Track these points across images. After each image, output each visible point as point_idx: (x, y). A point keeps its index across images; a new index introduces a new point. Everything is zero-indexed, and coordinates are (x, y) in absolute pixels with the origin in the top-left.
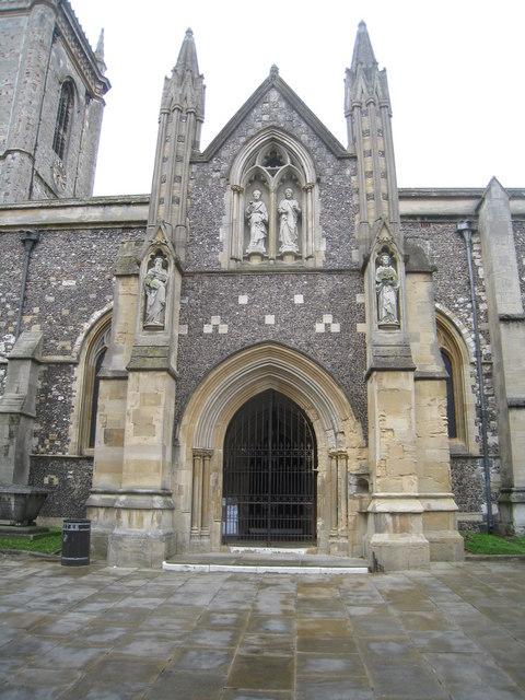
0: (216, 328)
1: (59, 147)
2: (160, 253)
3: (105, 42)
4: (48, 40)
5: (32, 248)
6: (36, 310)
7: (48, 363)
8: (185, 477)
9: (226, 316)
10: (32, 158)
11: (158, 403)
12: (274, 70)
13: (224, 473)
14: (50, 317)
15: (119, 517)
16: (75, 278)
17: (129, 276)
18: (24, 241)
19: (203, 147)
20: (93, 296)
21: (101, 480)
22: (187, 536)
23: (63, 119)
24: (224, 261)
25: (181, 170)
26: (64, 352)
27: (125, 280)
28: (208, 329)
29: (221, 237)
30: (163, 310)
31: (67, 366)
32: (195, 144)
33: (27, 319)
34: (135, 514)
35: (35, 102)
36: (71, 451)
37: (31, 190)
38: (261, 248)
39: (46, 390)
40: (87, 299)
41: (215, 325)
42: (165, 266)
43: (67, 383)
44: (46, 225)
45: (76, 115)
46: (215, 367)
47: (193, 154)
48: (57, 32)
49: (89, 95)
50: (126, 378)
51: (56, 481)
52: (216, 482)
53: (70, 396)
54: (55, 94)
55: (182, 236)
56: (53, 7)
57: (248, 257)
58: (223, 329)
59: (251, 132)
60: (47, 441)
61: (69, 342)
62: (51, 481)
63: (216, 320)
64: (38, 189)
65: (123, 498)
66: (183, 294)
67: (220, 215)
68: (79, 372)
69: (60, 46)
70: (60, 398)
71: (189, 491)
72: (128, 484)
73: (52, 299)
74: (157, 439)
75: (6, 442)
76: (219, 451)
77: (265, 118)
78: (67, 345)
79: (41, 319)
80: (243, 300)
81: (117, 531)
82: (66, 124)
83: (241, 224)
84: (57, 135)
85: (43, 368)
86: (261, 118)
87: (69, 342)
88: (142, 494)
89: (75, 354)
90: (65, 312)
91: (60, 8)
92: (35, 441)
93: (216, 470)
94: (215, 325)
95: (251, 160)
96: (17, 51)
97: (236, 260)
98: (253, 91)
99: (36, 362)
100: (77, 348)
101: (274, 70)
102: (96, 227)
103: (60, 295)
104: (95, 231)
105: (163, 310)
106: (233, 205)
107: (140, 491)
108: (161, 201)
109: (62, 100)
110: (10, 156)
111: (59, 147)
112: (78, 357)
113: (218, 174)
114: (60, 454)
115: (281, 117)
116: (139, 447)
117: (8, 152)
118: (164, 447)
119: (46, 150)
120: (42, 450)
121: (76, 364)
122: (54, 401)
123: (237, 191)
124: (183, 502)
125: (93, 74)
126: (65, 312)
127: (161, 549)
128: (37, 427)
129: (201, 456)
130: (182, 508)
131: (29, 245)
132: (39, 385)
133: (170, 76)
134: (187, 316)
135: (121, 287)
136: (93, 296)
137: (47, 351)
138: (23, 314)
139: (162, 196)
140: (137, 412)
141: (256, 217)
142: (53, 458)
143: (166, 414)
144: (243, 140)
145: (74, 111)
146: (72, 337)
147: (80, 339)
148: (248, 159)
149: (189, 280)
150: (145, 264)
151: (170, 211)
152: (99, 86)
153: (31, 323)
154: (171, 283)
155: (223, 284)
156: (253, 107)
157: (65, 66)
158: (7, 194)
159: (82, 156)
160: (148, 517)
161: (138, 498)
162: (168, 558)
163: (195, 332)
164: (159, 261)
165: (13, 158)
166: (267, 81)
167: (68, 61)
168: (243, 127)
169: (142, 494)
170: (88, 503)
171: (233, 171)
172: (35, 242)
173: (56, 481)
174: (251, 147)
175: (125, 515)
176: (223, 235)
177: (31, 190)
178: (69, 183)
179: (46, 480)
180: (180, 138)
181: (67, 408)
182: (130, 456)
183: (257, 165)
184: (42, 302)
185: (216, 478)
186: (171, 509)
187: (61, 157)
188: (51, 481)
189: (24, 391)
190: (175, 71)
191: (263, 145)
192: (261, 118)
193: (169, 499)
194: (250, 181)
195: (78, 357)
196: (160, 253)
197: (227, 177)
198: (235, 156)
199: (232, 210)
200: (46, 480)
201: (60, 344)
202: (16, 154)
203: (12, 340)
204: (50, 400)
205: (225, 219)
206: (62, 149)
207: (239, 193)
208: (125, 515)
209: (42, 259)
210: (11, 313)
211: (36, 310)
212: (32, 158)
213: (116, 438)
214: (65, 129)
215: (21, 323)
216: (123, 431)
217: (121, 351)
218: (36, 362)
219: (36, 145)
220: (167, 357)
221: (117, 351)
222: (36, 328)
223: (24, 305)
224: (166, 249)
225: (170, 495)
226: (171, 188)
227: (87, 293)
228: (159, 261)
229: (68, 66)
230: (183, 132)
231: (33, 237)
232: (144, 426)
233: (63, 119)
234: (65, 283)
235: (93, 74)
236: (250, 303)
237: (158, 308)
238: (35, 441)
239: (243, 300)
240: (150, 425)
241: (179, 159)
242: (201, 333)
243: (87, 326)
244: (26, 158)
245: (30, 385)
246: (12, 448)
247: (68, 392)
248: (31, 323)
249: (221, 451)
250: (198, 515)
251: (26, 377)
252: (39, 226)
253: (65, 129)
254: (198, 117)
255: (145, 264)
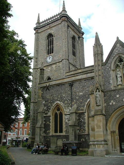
0: (48, 140)
1: (74, 54)
2: (97, 89)
3: (81, 22)
4: (66, 29)
5: (72, 87)
6: (75, 101)
7: (79, 113)
8: (109, 137)
9: (114, 100)
10: (68, 60)
11: (101, 122)
12: (118, 38)
13: (119, 135)
14: (78, 102)
15: (95, 146)
16: (82, 92)
17: (92, 94)
18: (70, 85)
19: (104, 61)
20: (87, 96)
21: (92, 139)
22: (111, 151)
23: (74, 46)
24: (112, 88)
25: (100, 68)
26: (82, 110)
27: (92, 95)
28: (111, 104)
29: (111, 82)
30: (100, 101)
31: (83, 113)
32: (102, 60)
33: (73, 103)
34: (99, 145)
35: (66, 46)
36: (86, 133)
37: (69, 67)
38: (121, 83)
39: (79, 119)
40: (86, 97)
41: (112, 102)
42: (99, 91)
43: (84, 117)
44: (74, 81)
45: (77, 44)
46: (113, 112)
47: (102, 63)
48: (68, 26)
49: (79, 38)
50: (94, 117)
51: (84, 140)
52: (117, 138)
53: (85, 120)
54: (71, 41)
55: (102, 83)
56: (66, 21)
57: (118, 85)
58: (114, 103)
59: (114, 56)
60: (81, 131)
61: (83, 108)
62: (83, 140)
63: (112, 101)
64: (71, 67)
65: (96, 142)
66: (104, 96)
67: (110, 77)
68: (86, 114)
69: (70, 29)
70: (83, 121)
71: (111, 140)
72: (96, 140)
73: (78, 98)
74: (102, 129)
75: (72, 132)
76: (117, 131)
77: (117, 51)
78: (83, 108)
79: (76, 103)
80: (118, 96)
81: (95, 149)
82: (75, 47)
83: (115, 78)
84: (73, 51)
85: (78, 114)
86: (116, 52)
87: (83, 108)
88: (100, 141)
89: (85, 110)
90: (81, 101)
91: (68, 20)
92: (78, 131)
93: (117, 135)
94: (112, 102)
95: (115, 62)
96: (60, 34)
97: (115, 87)
98: (107, 56)
99: (76, 113)
100: (85, 109)
101: (118, 38)
102: (85, 79)
103: (80, 97)
104: (85, 80)
105: (100, 101)
106: (112, 74)
107: (99, 141)
108: (96, 76)
109: (73, 42)
110: (63, 61)
111: (74, 54)
112: (86, 111)
113: (108, 67)
114: (84, 134)
115: (120, 50)
116: (98, 131)
117: (62, 60)
118: (103, 131)
119: (71, 56)
120: (80, 133)
121: (85, 112)
122: (81, 122)
123: (114, 71)
124: (110, 143)
125: (79, 32)
126: (81, 101)
127: (104, 153)
128: (78, 128)
129: (113, 132)
130: (109, 144)
131: (71, 86)
132: (78, 118)
133: (94, 45)
134: (106, 101)
135: (91, 96)
136: (87, 96)
137: (78, 110)
138: (72, 102)
139: (97, 75)
140: (97, 124)
141: (118, 76)
142: (83, 135)
143: (103, 124)
144: (113, 58)
145: (76, 43)
146: (83, 106)
147: (85, 106)
148: (115, 62)
149: (105, 93)
150: (95, 92)
151: (99, 78)
152: (81, 34)
153: (74, 104)
154: (101, 95)
155: (113, 93)
156: (114, 49)
157: (72, 33)
158: (64, 70)
159: (80, 54)
160: (101, 146)
161: (99, 142)
162: (106, 155)
163: (108, 105)
164: (98, 90)
165: (64, 61)
166: (116, 42)
167: (72, 31)
168: (112, 54)
169: (100, 141)
170: (89, 144)
171: (111, 66)
172: (72, 85)
173: (84, 140)
174: (115, 59)
175: (96, 146)
176: (111, 82)
177: (69, 67)
178: (78, 62)
179: (82, 140)
180: (98, 60)
181: (84, 123)
182: (96, 134)
183: (117, 63)
184: (76, 99)
185: (117, 137)
186: (107, 144)
187: (75, 56)
188: (83, 140)
189: (74, 120)
190: (95, 45)
191: (118, 58)
192: (116, 52)
193: (106, 142)
194: (116, 67)
195: (86, 111)
196: (97, 89)
197: (110, 67)
198: (111, 62)
199: (112, 75)
200: (82, 140)
201: (81, 108)
202: (64, 60)
203: (70, 108)
204: (81, 121)
205: (111, 78)
206: (75, 54)
207: (114, 71)
208: (96, 146)
209: (74, 89)
210: (69, 102)
211: (75, 101)
212: (68, 60)
213: (93, 130)
214: (75, 49)
215: (72, 105)
216: (94, 128)
217: (93, 111)
218: (76, 113)
219: (69, 56)
220: (102, 111)
221: (92, 111)
222: (75, 105)
223: (72, 100)
224: (99, 87)
225: (106, 141)
226: (98, 73)
227: (85, 95)
228: (98, 90)
229: (72, 33)
230: (99, 59)
231: (72, 84)
232: (99, 127)
233: (74, 46)
234: (80, 94)
235: (79, 32)
236: (120, 96)
237: (99, 101)
238: (78, 131)
239: (118, 96)
240: (100, 126)
241: (99, 65)
242: (109, 105)
243: (86, 103)
244: (67, 60)
245: (75, 119)
246: (73, 133)
247: (84, 119)
248: (74, 104)
249: (118, 131)
250: (113, 146)
251: (74, 117)
252: (72, 81)
253: (75, 49)
254: (102, 54)
255: (95, 92)
